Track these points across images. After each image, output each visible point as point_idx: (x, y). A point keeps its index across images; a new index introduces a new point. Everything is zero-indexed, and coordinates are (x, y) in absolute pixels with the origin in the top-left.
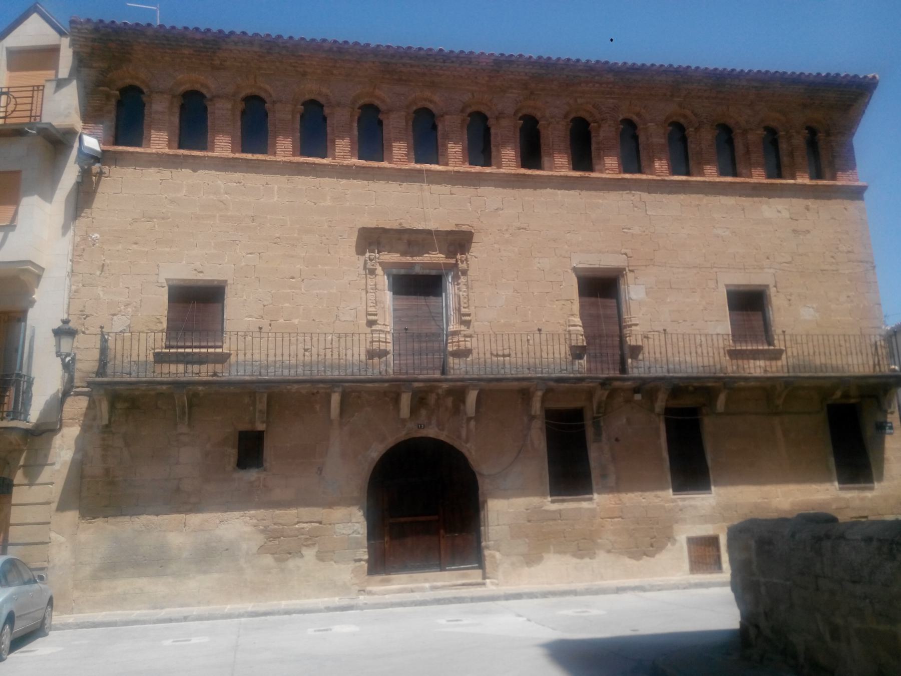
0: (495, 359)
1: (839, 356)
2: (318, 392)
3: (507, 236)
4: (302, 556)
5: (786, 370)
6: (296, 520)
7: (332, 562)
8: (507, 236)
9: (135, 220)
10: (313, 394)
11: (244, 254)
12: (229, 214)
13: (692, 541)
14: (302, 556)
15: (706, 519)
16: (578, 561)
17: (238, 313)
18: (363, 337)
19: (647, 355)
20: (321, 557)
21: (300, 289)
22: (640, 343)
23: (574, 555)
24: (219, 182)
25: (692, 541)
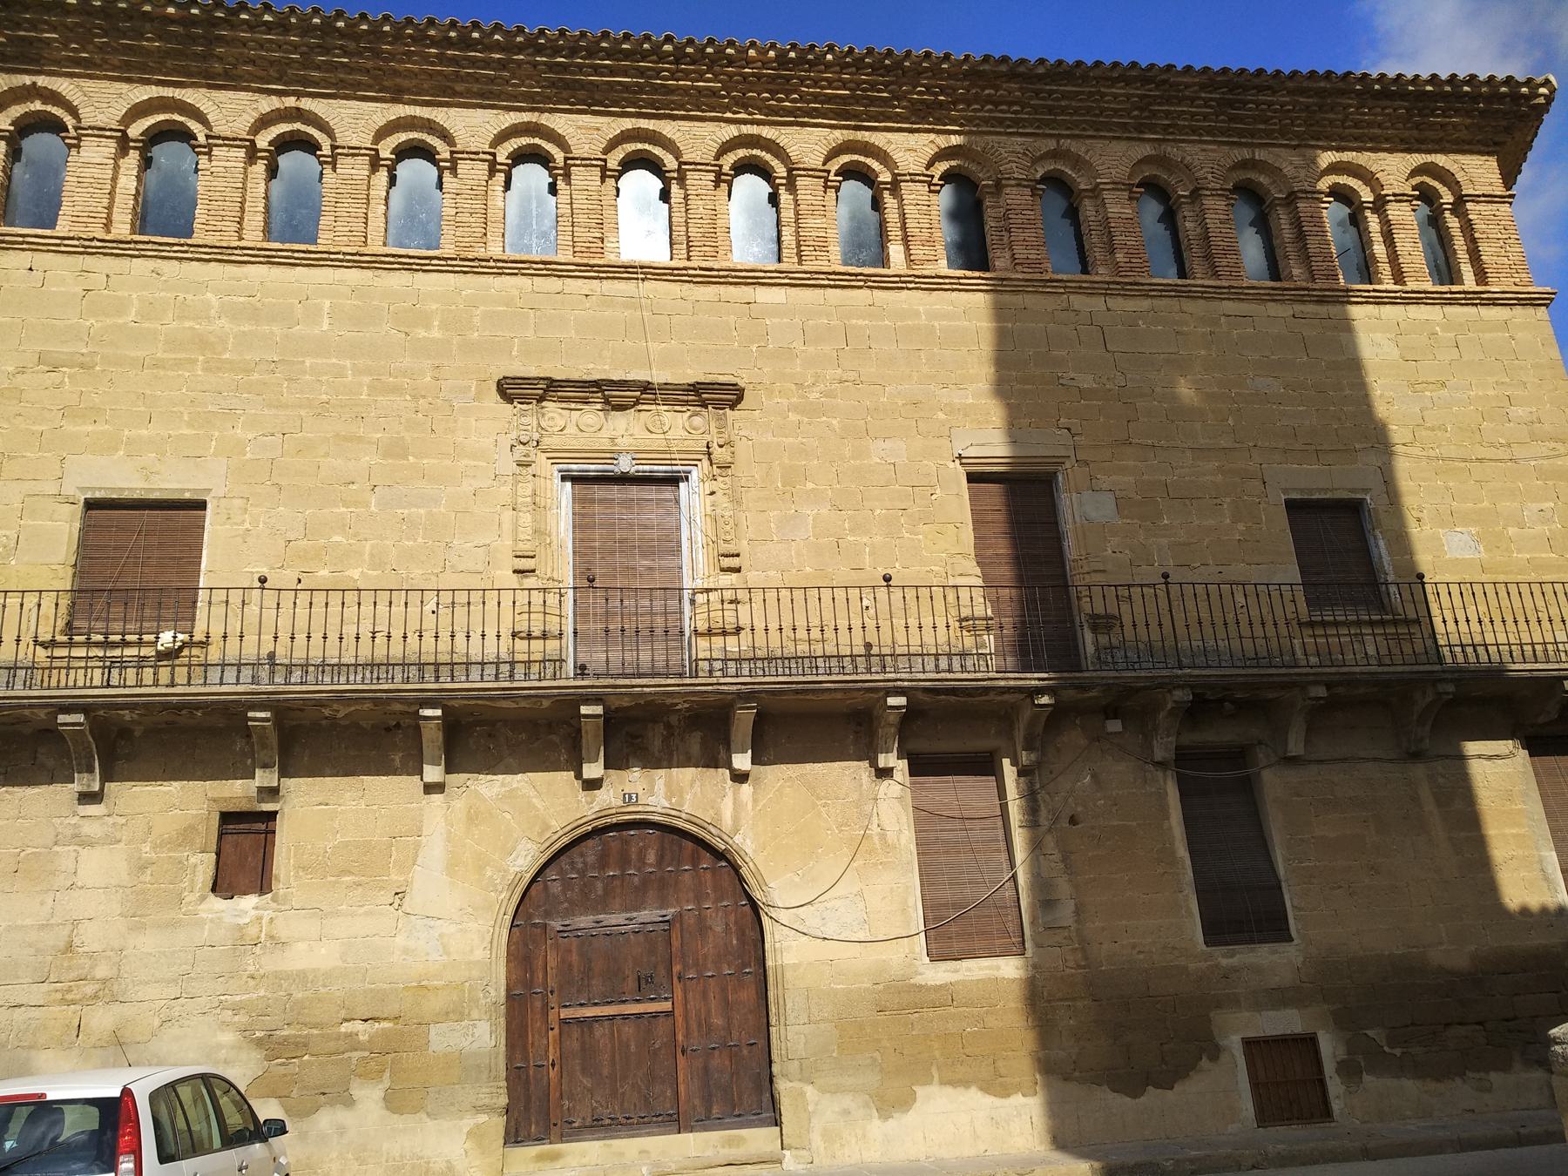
0: (521, 645)
1: (1522, 625)
2: (398, 726)
3: (813, 396)
4: (349, 1102)
5: (1172, 662)
6: (343, 1014)
7: (424, 1116)
8: (813, 396)
9: (22, 370)
10: (388, 729)
11: (250, 436)
12: (227, 356)
13: (1251, 1045)
14: (349, 1102)
15: (1280, 998)
16: (997, 1101)
17: (223, 555)
18: (507, 598)
19: (1129, 632)
20: (394, 1102)
21: (368, 506)
22: (1113, 610)
23: (987, 1089)
24: (209, 295)
25: (1251, 1045)
